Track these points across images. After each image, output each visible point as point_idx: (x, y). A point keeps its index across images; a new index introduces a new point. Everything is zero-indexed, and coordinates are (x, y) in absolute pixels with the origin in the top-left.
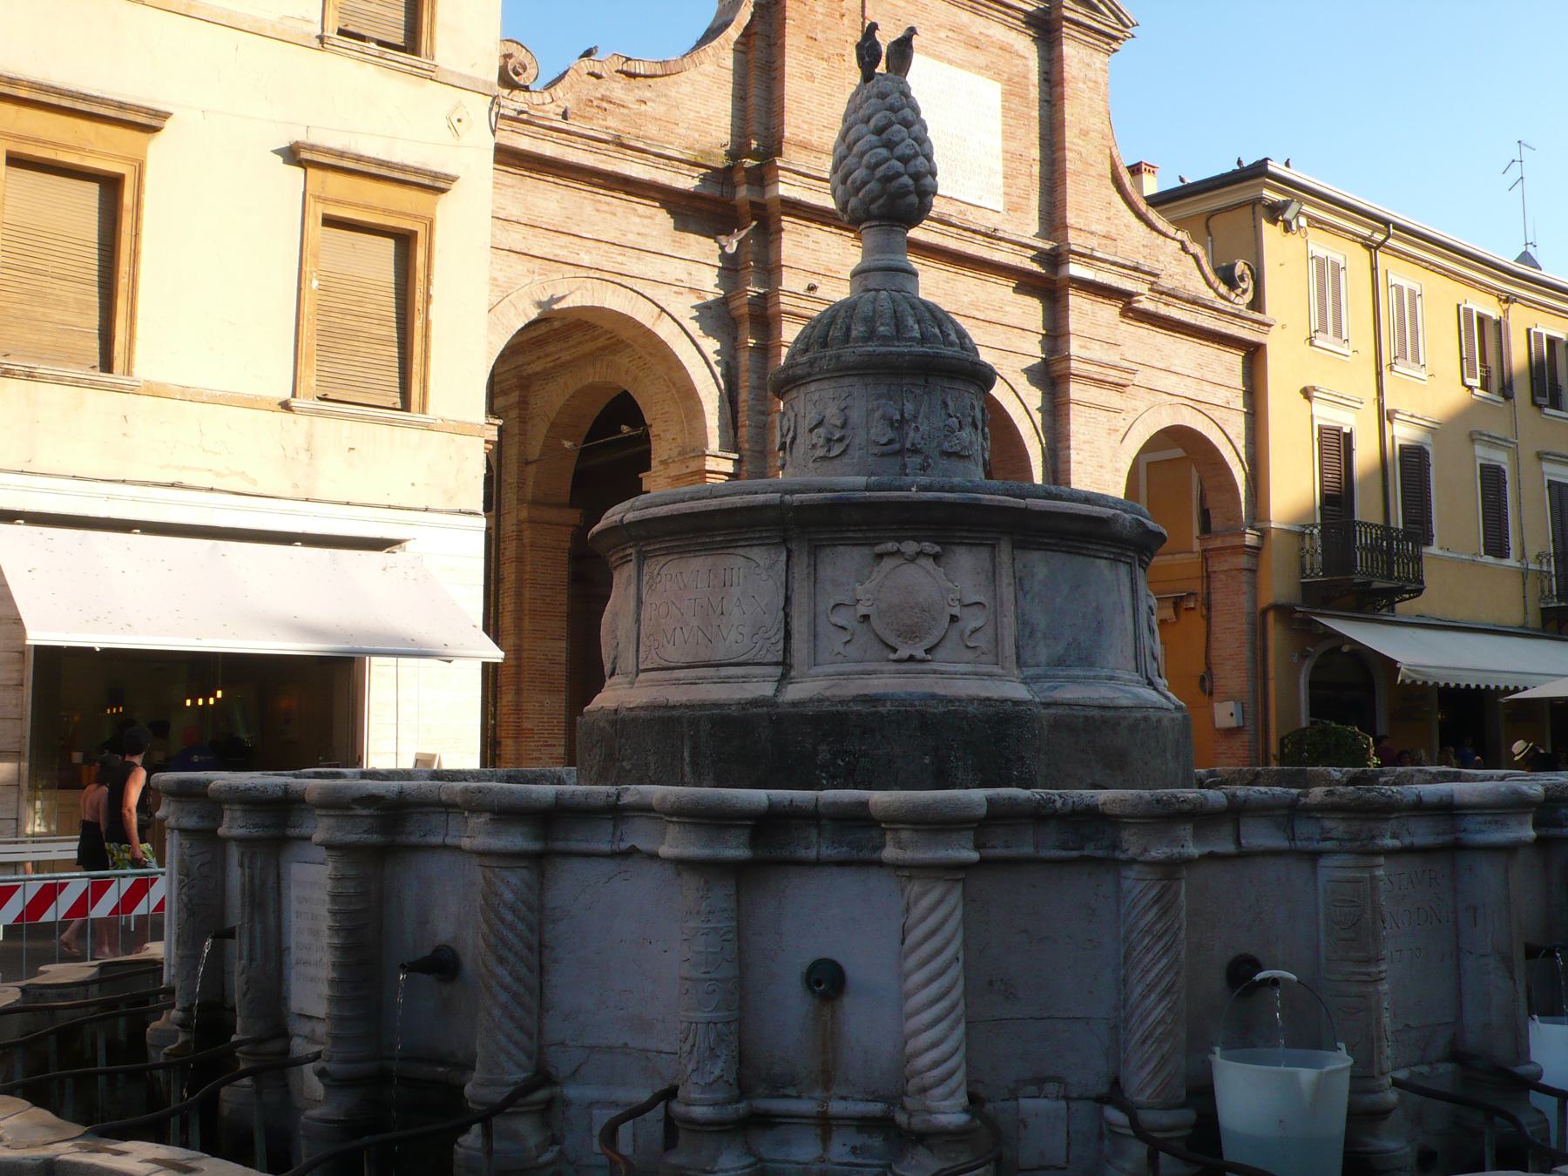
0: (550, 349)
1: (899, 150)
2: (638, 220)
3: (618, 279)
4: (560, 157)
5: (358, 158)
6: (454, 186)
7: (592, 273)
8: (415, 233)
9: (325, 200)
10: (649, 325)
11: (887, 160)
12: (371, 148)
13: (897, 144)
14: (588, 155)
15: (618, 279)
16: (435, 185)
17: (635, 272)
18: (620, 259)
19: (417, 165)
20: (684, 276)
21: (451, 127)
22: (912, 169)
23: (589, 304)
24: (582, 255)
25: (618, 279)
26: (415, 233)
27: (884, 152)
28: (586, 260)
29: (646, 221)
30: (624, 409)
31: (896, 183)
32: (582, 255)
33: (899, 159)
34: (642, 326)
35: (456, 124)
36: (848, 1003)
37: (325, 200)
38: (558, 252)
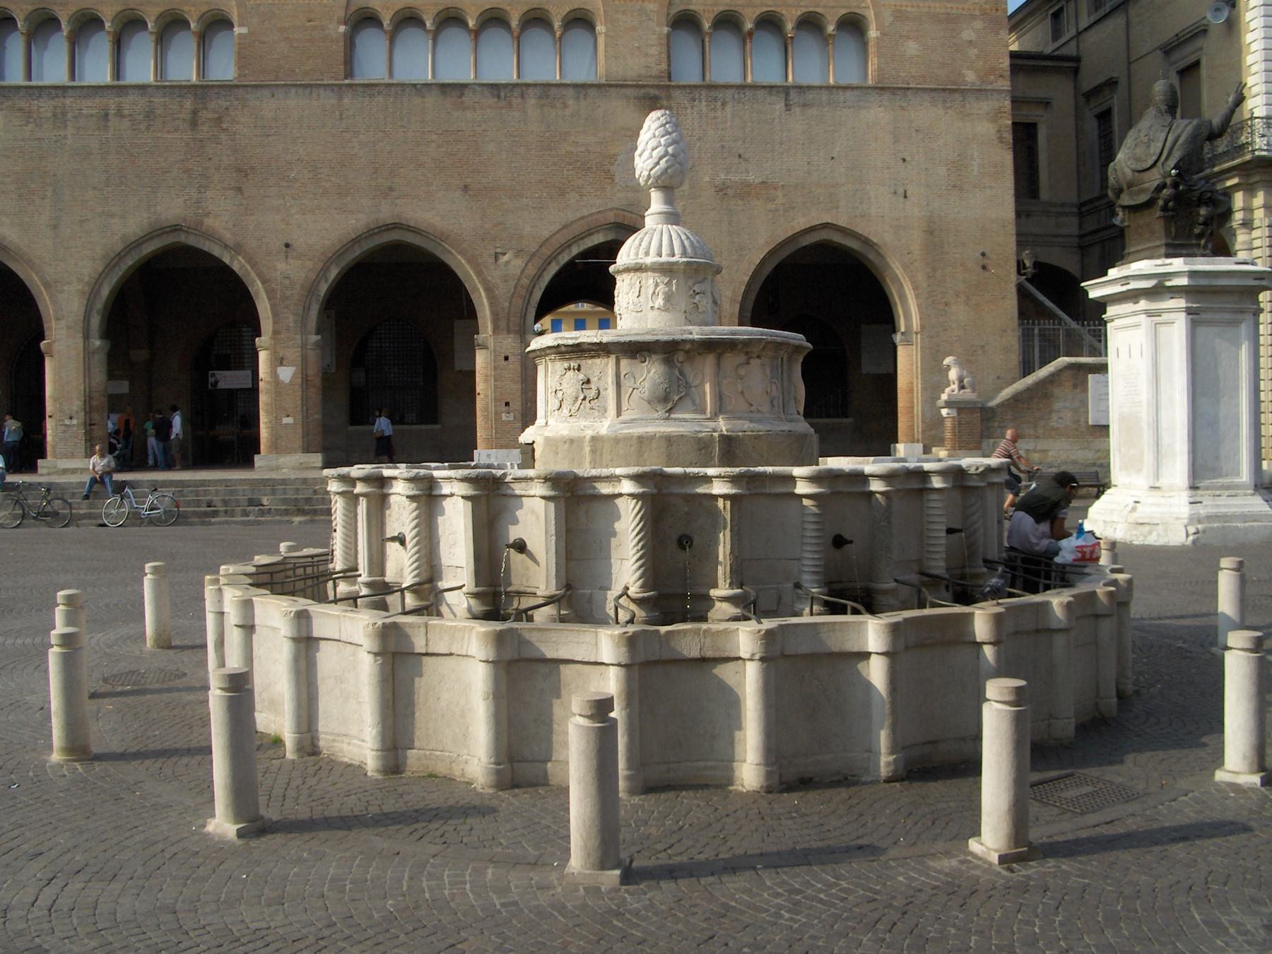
36: (529, 546)
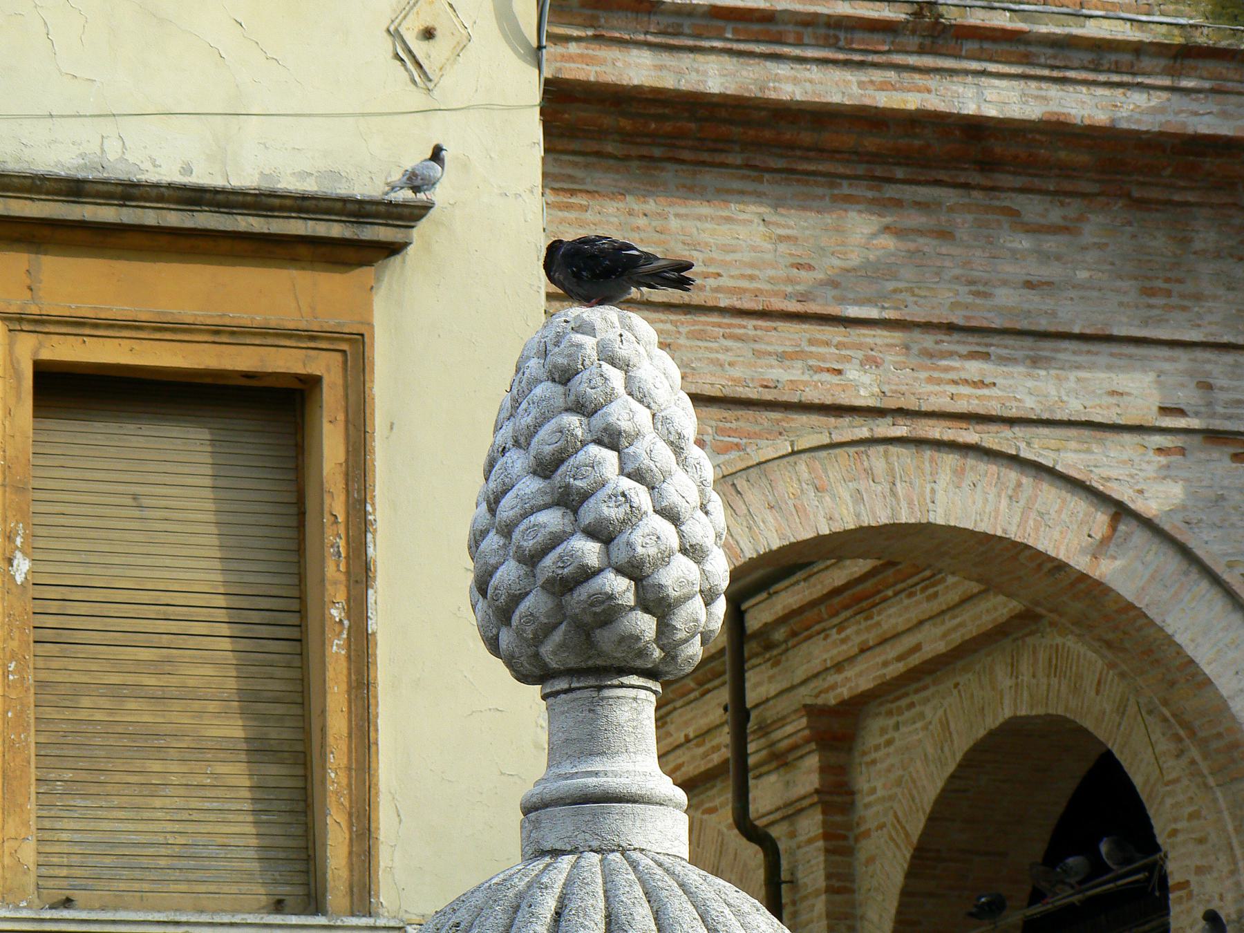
0: (892, 617)
1: (588, 514)
2: (1024, 243)
3: (970, 435)
4: (753, 91)
5: (129, 192)
6: (420, 232)
7: (884, 428)
8: (314, 382)
9: (39, 323)
10: (1081, 563)
11: (556, 540)
12: (167, 154)
13: (585, 496)
14: (837, 74)
15: (967, 437)
16: (360, 234)
17: (1030, 405)
18: (974, 368)
19: (309, 186)
20: (1186, 396)
21: (406, 57)
22: (620, 555)
23: (883, 517)
24: (853, 373)
25: (970, 435)
26: (314, 382)
27: (552, 519)
28: (862, 386)
29: (1051, 243)
30: (1105, 807)
31: (583, 592)
32: (853, 373)
33: (592, 533)
34: (1060, 567)
35: (419, 47)
37: (39, 323)
38: (777, 373)
